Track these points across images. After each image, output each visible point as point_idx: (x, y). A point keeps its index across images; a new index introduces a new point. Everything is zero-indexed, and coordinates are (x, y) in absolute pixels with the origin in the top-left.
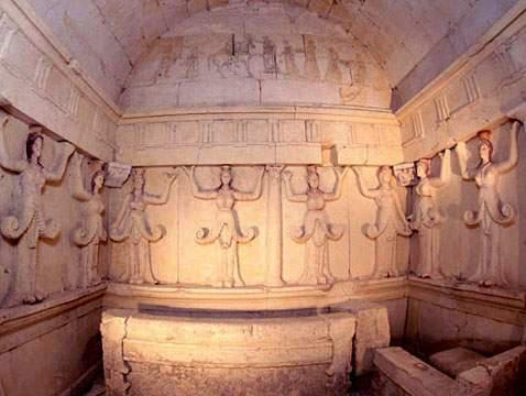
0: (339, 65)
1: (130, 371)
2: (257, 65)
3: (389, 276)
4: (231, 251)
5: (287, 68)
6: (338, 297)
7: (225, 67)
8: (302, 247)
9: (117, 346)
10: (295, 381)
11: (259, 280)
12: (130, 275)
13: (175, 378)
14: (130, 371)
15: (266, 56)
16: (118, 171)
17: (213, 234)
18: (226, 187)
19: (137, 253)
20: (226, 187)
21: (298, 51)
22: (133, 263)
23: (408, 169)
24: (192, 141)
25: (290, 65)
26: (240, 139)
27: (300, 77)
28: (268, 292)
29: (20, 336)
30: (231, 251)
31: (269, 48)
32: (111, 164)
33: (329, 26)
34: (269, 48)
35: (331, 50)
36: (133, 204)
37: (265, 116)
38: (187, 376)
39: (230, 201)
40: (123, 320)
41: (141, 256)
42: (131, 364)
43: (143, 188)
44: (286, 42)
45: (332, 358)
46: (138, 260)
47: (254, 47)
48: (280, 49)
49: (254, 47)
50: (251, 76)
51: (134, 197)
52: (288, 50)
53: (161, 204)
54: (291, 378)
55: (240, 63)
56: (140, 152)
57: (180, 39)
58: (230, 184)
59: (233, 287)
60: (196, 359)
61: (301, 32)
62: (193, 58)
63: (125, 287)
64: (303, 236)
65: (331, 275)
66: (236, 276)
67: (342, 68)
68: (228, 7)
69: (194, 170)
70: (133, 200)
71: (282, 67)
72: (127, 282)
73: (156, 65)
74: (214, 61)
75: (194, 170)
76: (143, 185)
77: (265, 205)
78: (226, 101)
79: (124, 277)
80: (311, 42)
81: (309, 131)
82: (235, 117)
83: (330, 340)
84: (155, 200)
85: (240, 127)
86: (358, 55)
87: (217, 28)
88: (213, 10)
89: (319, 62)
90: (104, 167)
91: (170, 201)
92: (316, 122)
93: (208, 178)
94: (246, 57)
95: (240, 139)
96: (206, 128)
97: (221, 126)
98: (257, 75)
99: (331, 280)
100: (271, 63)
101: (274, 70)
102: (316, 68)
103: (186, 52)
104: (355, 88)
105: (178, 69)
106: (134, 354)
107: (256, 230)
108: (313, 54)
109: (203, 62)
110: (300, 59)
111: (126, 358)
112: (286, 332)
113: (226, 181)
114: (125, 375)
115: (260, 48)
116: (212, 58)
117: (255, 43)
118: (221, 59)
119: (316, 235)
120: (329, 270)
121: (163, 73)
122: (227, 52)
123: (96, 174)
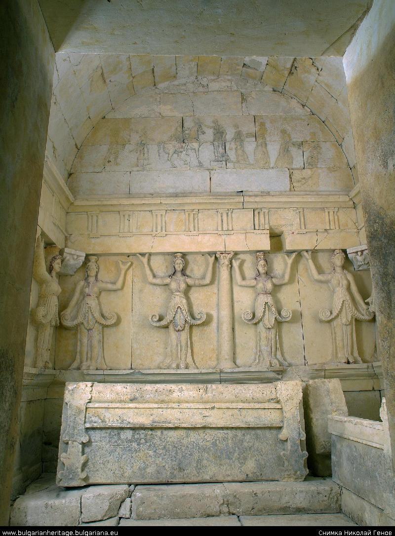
0: (290, 149)
2: (207, 153)
4: (184, 335)
5: (237, 156)
7: (175, 155)
9: (80, 411)
13: (134, 445)
15: (216, 143)
16: (75, 256)
18: (179, 274)
19: (90, 338)
20: (179, 274)
21: (249, 135)
22: (85, 349)
23: (362, 251)
24: (146, 230)
25: (240, 152)
26: (192, 229)
27: (250, 164)
31: (219, 133)
32: (66, 250)
33: (283, 102)
34: (219, 133)
35: (284, 132)
37: (215, 207)
39: (183, 286)
40: (89, 384)
41: (95, 342)
43: (96, 276)
44: (236, 126)
45: (282, 421)
46: (91, 346)
47: (204, 133)
48: (230, 134)
49: (204, 133)
50: (200, 165)
51: (89, 283)
52: (239, 137)
53: (115, 291)
54: (245, 444)
55: (190, 152)
56: (93, 241)
57: (127, 121)
58: (182, 270)
61: (253, 113)
62: (142, 145)
64: (254, 321)
65: (285, 360)
67: (294, 151)
68: (176, 83)
69: (149, 260)
71: (232, 155)
73: (104, 149)
74: (164, 148)
75: (149, 260)
76: (97, 273)
77: (216, 291)
78: (178, 191)
80: (262, 124)
82: (186, 208)
83: (278, 402)
84: (110, 286)
85: (192, 216)
86: (314, 134)
87: (166, 110)
89: (270, 147)
90: (61, 252)
91: (125, 288)
92: (264, 210)
93: (160, 266)
95: (192, 229)
96: (159, 218)
97: (174, 216)
98: (206, 164)
100: (221, 150)
101: (223, 159)
102: (266, 154)
103: (135, 138)
104: (307, 172)
105: (128, 156)
108: (264, 138)
109: (153, 149)
110: (250, 146)
112: (237, 391)
113: (179, 267)
115: (209, 134)
116: (161, 144)
117: (205, 129)
118: (171, 147)
119: (266, 317)
120: (283, 355)
121: (112, 159)
122: (177, 139)
123: (54, 258)
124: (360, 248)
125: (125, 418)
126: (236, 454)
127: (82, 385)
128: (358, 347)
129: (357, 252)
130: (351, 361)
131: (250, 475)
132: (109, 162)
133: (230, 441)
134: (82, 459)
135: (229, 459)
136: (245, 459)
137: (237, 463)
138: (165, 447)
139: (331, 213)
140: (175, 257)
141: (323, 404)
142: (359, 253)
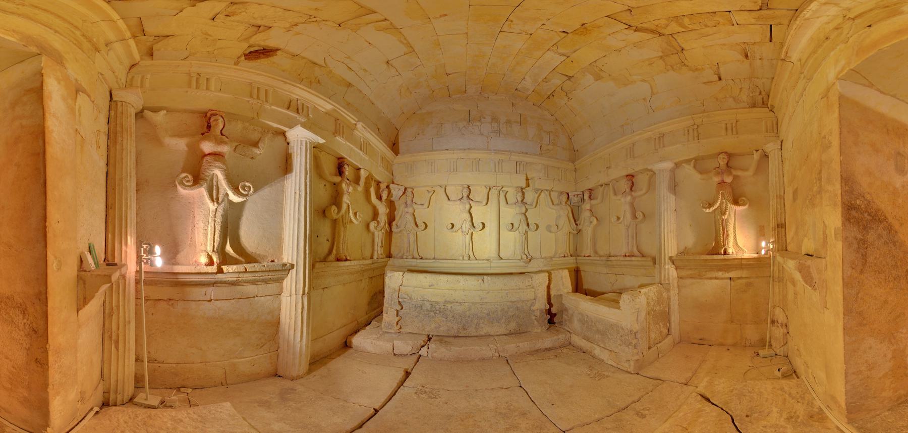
1: (402, 309)
3: (564, 257)
6: (533, 266)
8: (512, 233)
10: (513, 316)
11: (486, 256)
12: (404, 254)
13: (432, 314)
14: (402, 309)
17: (456, 227)
23: (578, 195)
28: (80, 305)
29: (716, 218)
30: (468, 237)
36: (406, 209)
38: (440, 312)
40: (401, 273)
42: (402, 304)
59: (469, 259)
60: (448, 300)
63: (401, 261)
66: (471, 254)
70: (406, 207)
72: (402, 258)
79: (400, 255)
81: (518, 167)
88: (453, 97)
94: (478, 124)
99: (529, 257)
101: (498, 132)
106: (406, 297)
107: (484, 225)
111: (400, 300)
114: (397, 311)
115: (489, 119)
124: (576, 193)
125: (425, 297)
126: (503, 321)
127: (396, 274)
128: (720, 270)
129: (574, 195)
130: (566, 255)
131: (512, 331)
132: (418, 134)
133: (499, 313)
134: (397, 319)
135: (498, 322)
136: (509, 322)
137: (503, 325)
138: (453, 317)
139: (563, 171)
140: (262, 343)
141: (23, 72)
142: (576, 196)
